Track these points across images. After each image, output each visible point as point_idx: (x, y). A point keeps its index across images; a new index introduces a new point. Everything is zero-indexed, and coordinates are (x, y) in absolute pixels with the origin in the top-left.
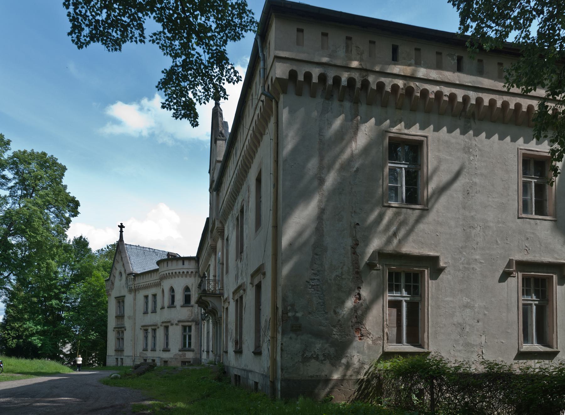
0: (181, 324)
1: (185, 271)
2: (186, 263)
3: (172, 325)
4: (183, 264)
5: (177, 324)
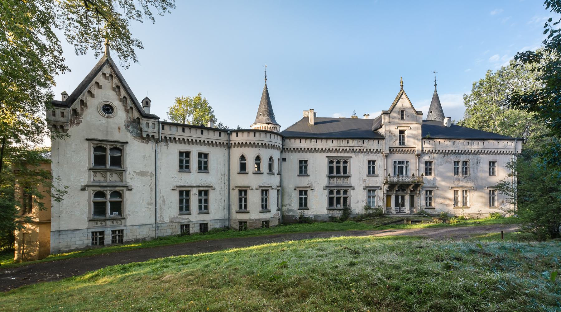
0: (299, 189)
1: (214, 141)
2: (257, 134)
3: (252, 189)
4: (255, 136)
5: (257, 189)
